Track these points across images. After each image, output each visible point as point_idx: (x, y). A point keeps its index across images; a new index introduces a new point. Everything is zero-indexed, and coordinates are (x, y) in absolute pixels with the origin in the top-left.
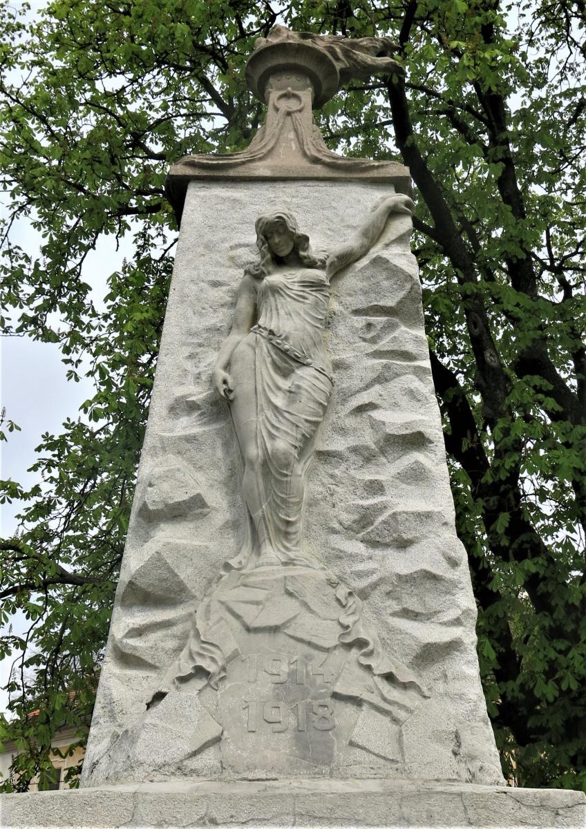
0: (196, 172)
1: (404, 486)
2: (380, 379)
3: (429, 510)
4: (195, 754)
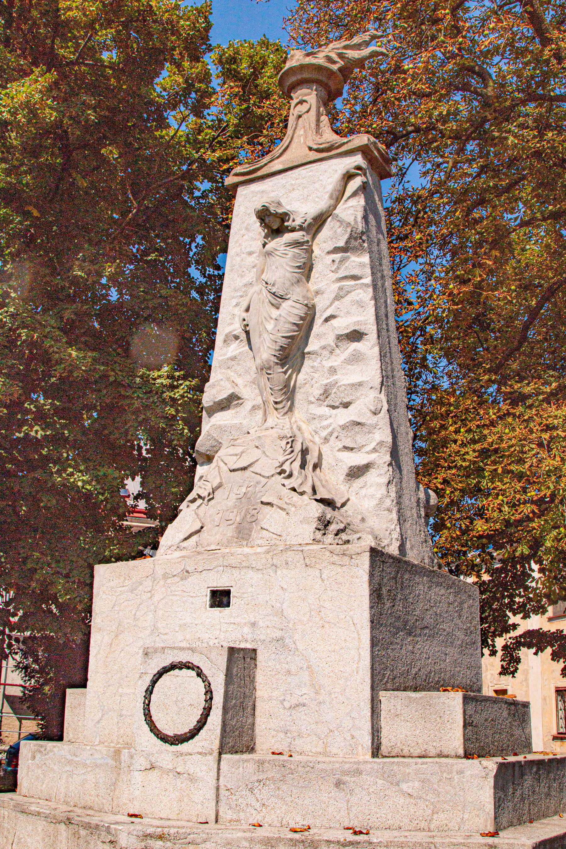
0: (241, 179)
1: (349, 367)
2: (338, 298)
3: (361, 380)
4: (186, 539)
